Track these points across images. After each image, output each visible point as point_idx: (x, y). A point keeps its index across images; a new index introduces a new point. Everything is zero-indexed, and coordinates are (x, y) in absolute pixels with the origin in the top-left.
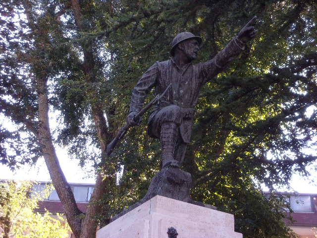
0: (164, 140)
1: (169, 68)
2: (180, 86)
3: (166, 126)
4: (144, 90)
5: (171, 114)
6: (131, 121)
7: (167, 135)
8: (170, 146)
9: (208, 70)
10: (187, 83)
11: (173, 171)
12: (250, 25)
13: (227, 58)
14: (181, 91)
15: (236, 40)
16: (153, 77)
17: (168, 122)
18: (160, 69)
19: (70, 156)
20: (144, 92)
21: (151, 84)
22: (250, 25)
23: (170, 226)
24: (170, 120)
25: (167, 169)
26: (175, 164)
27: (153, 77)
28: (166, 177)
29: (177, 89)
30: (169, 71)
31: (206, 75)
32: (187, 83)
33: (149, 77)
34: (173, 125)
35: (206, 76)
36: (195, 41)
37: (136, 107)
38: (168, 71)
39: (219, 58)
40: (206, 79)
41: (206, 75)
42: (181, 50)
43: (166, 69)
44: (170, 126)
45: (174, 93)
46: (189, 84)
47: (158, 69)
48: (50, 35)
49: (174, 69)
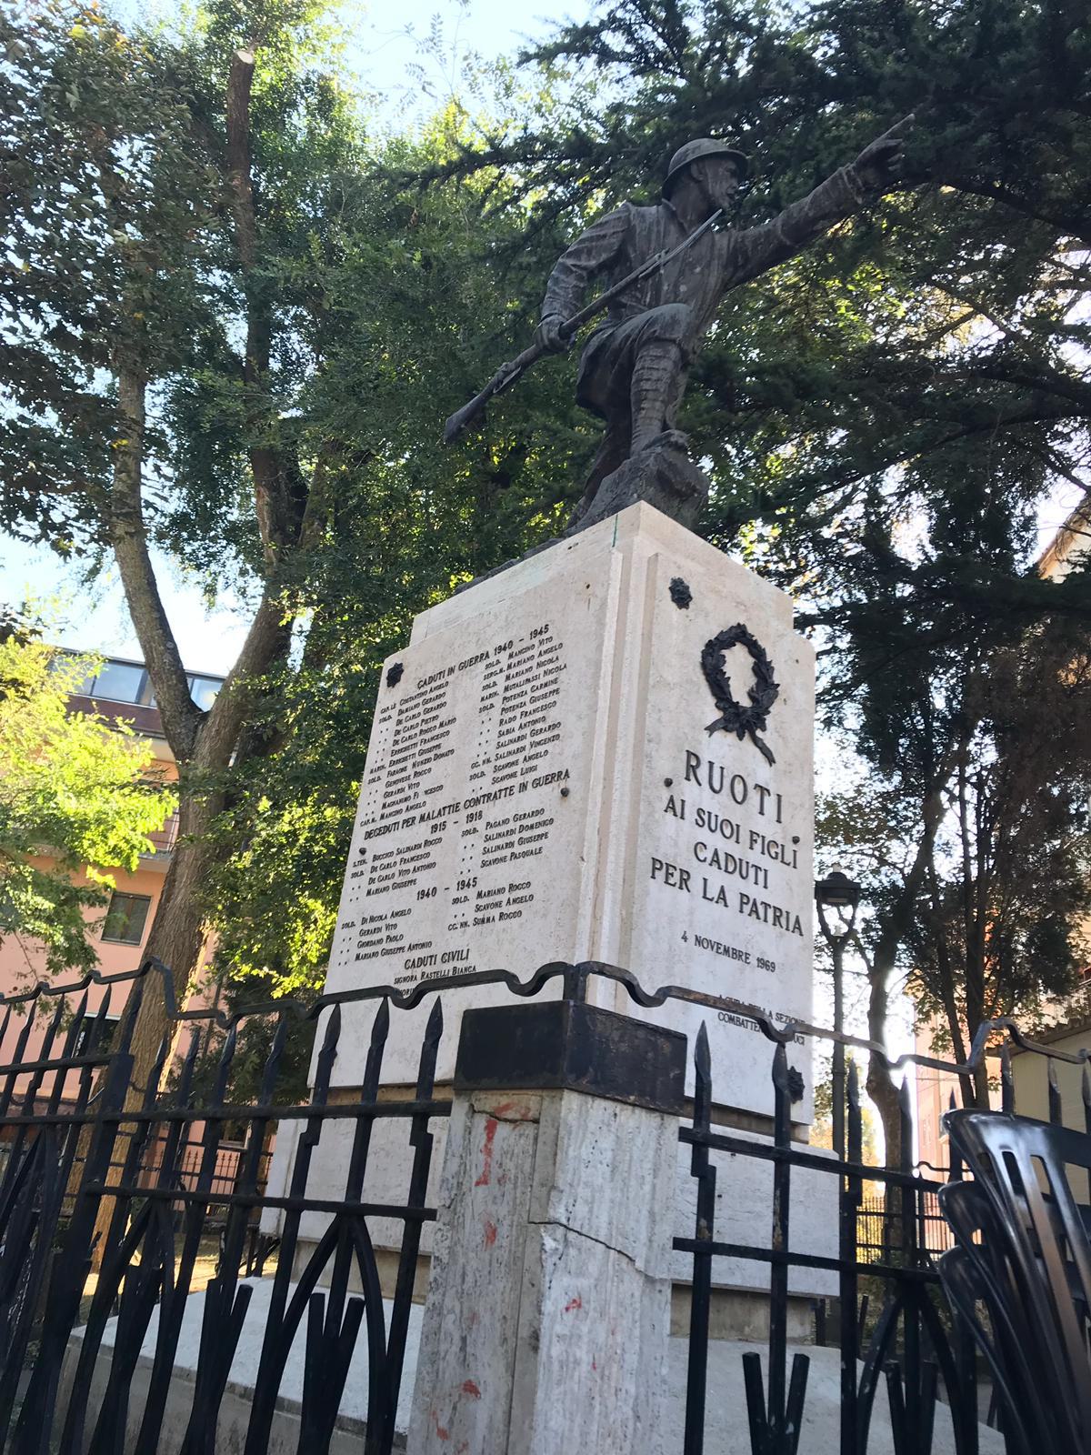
0: (646, 386)
1: (658, 223)
2: (682, 273)
3: (655, 351)
4: (584, 268)
5: (674, 321)
6: (552, 335)
7: (655, 375)
8: (658, 404)
9: (755, 248)
10: (698, 270)
11: (672, 456)
12: (893, 136)
13: (815, 221)
14: (683, 288)
15: (848, 173)
16: (613, 240)
17: (659, 340)
18: (635, 222)
19: (206, 598)
20: (585, 274)
21: (604, 256)
22: (893, 136)
23: (677, 576)
24: (667, 336)
25: (659, 450)
26: (681, 441)
27: (613, 240)
28: (655, 468)
29: (673, 280)
30: (658, 232)
31: (747, 260)
32: (698, 270)
33: (604, 236)
34: (674, 352)
35: (743, 266)
36: (732, 166)
37: (565, 306)
38: (655, 229)
39: (789, 217)
40: (740, 274)
41: (747, 260)
42: (698, 182)
43: (651, 224)
44: (668, 352)
45: (665, 288)
46: (702, 272)
47: (628, 220)
48: (197, 348)
49: (673, 228)
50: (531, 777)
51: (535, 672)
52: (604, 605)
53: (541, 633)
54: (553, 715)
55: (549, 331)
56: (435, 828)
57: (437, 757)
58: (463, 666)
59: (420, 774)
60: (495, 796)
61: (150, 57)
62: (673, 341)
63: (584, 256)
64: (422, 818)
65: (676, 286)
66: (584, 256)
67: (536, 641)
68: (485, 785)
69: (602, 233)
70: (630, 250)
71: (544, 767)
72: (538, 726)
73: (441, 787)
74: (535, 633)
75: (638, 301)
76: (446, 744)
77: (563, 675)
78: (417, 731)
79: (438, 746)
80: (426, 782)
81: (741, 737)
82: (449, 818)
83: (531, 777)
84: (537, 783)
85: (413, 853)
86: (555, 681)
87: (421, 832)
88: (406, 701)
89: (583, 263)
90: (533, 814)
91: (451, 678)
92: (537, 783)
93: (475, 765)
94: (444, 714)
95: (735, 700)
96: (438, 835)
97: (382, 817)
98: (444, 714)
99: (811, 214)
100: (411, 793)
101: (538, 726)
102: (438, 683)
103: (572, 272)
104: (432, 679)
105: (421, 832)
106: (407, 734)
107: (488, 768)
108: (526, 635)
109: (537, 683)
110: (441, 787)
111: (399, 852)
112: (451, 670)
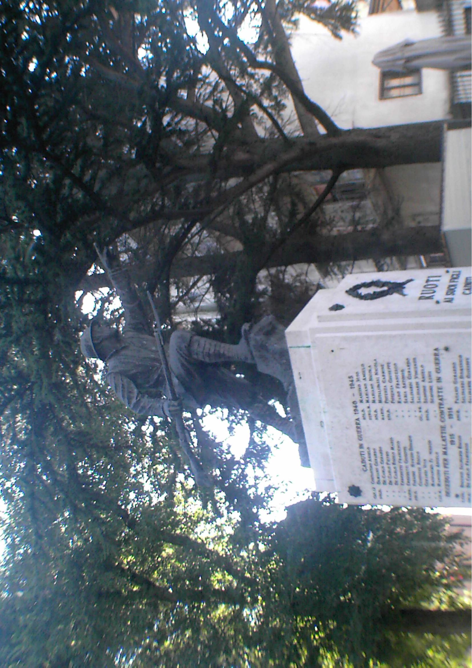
3: (195, 346)
4: (138, 395)
10: (145, 342)
14: (154, 348)
18: (117, 370)
47: (116, 373)
49: (123, 352)
50: (434, 375)
51: (374, 382)
52: (345, 339)
53: (352, 381)
54: (402, 365)
55: (173, 406)
56: (452, 443)
57: (411, 449)
58: (360, 438)
59: (419, 460)
60: (441, 400)
61: (118, 272)
62: (191, 337)
63: (132, 395)
64: (445, 453)
65: (152, 351)
66: (132, 395)
67: (356, 384)
68: (433, 408)
69: (121, 386)
70: (132, 372)
71: (430, 367)
72: (406, 374)
73: (430, 442)
74: (352, 386)
75: (158, 369)
76: (405, 443)
77: (380, 361)
78: (392, 466)
79: (405, 448)
80: (425, 455)
81: (404, 288)
82: (449, 431)
83: (434, 375)
84: (438, 370)
85: (464, 457)
86: (382, 366)
87: (453, 451)
88: (373, 479)
89: (135, 394)
90: (455, 370)
91: (365, 446)
92: (438, 370)
93: (421, 418)
94: (386, 448)
95: (298, 445)
96: (456, 440)
97: (439, 485)
98: (386, 448)
99: (127, 290)
100: (428, 464)
101: (406, 374)
102: (366, 456)
103: (139, 400)
104: (363, 461)
105: (453, 451)
106: (393, 474)
107: (425, 407)
108: (351, 391)
109: (381, 379)
110: (430, 442)
111: (461, 468)
112: (361, 446)
